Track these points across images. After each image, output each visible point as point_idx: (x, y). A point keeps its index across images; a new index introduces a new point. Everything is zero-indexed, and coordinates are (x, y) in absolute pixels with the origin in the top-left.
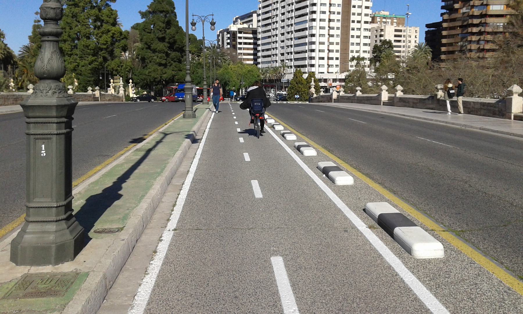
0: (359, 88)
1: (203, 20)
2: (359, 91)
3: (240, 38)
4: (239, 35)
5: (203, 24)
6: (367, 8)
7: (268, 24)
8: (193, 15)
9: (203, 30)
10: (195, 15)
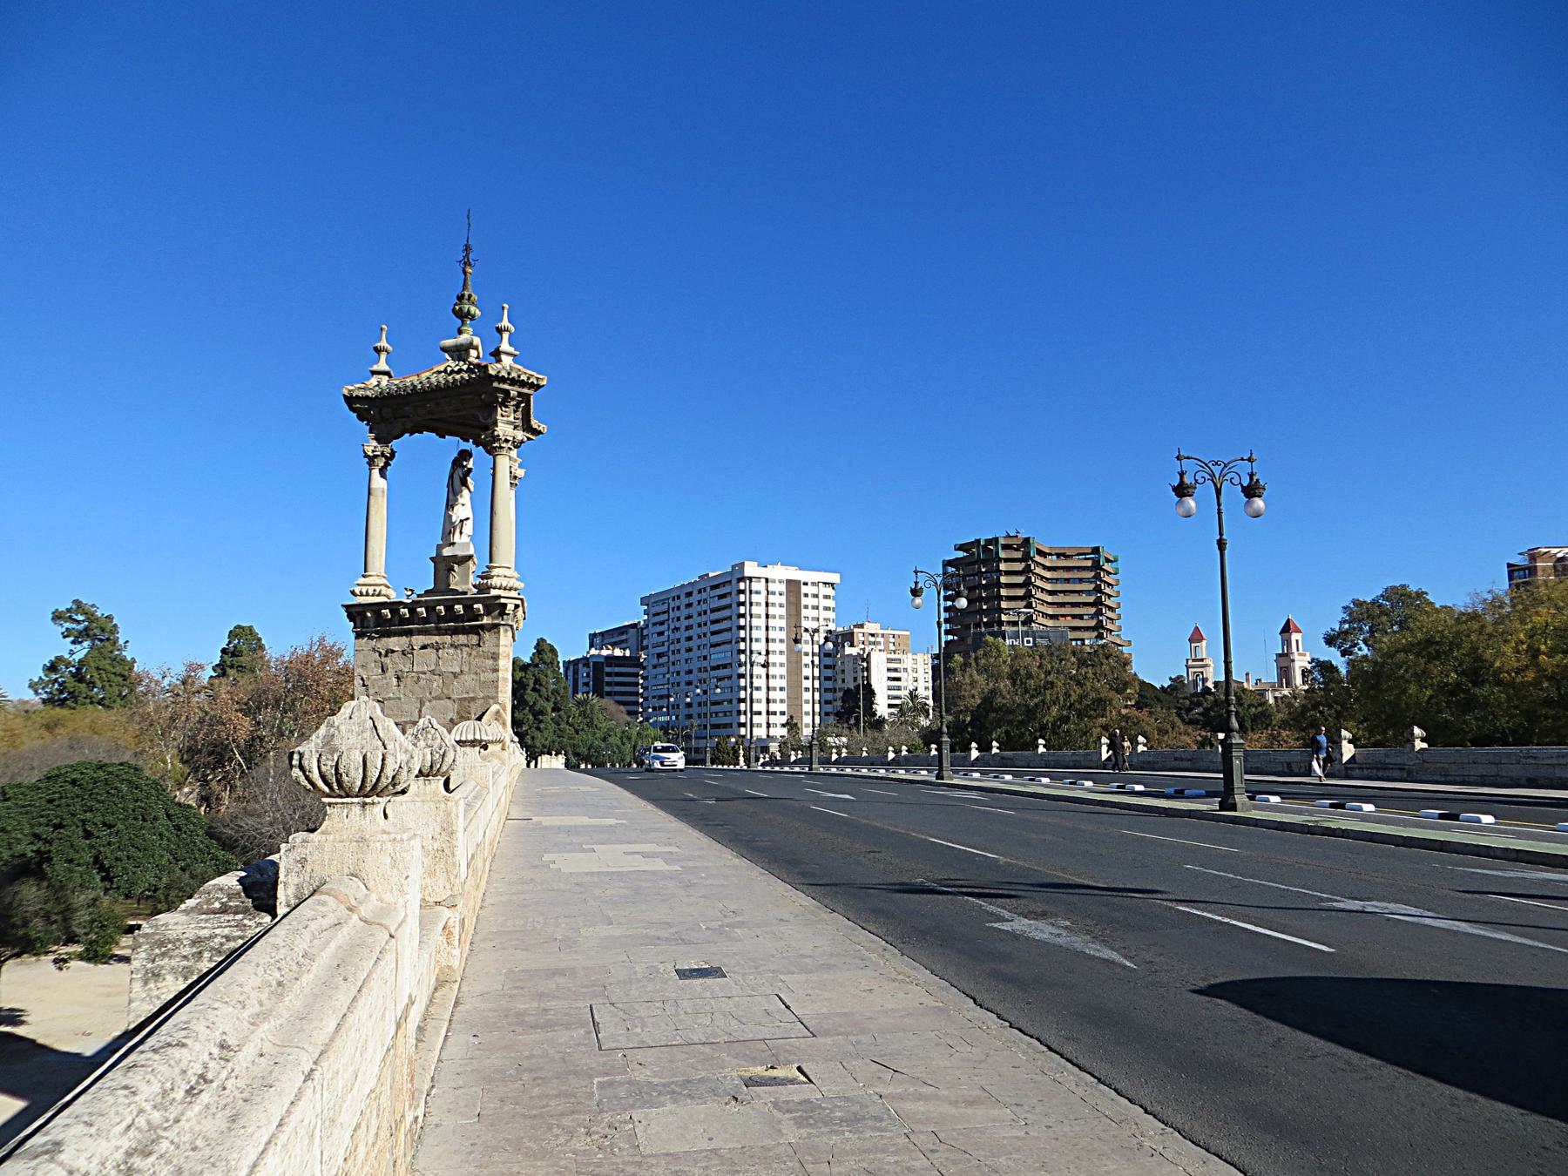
0: (1041, 741)
2: (1041, 747)
4: (607, 669)
5: (1218, 492)
6: (826, 609)
7: (1084, 567)
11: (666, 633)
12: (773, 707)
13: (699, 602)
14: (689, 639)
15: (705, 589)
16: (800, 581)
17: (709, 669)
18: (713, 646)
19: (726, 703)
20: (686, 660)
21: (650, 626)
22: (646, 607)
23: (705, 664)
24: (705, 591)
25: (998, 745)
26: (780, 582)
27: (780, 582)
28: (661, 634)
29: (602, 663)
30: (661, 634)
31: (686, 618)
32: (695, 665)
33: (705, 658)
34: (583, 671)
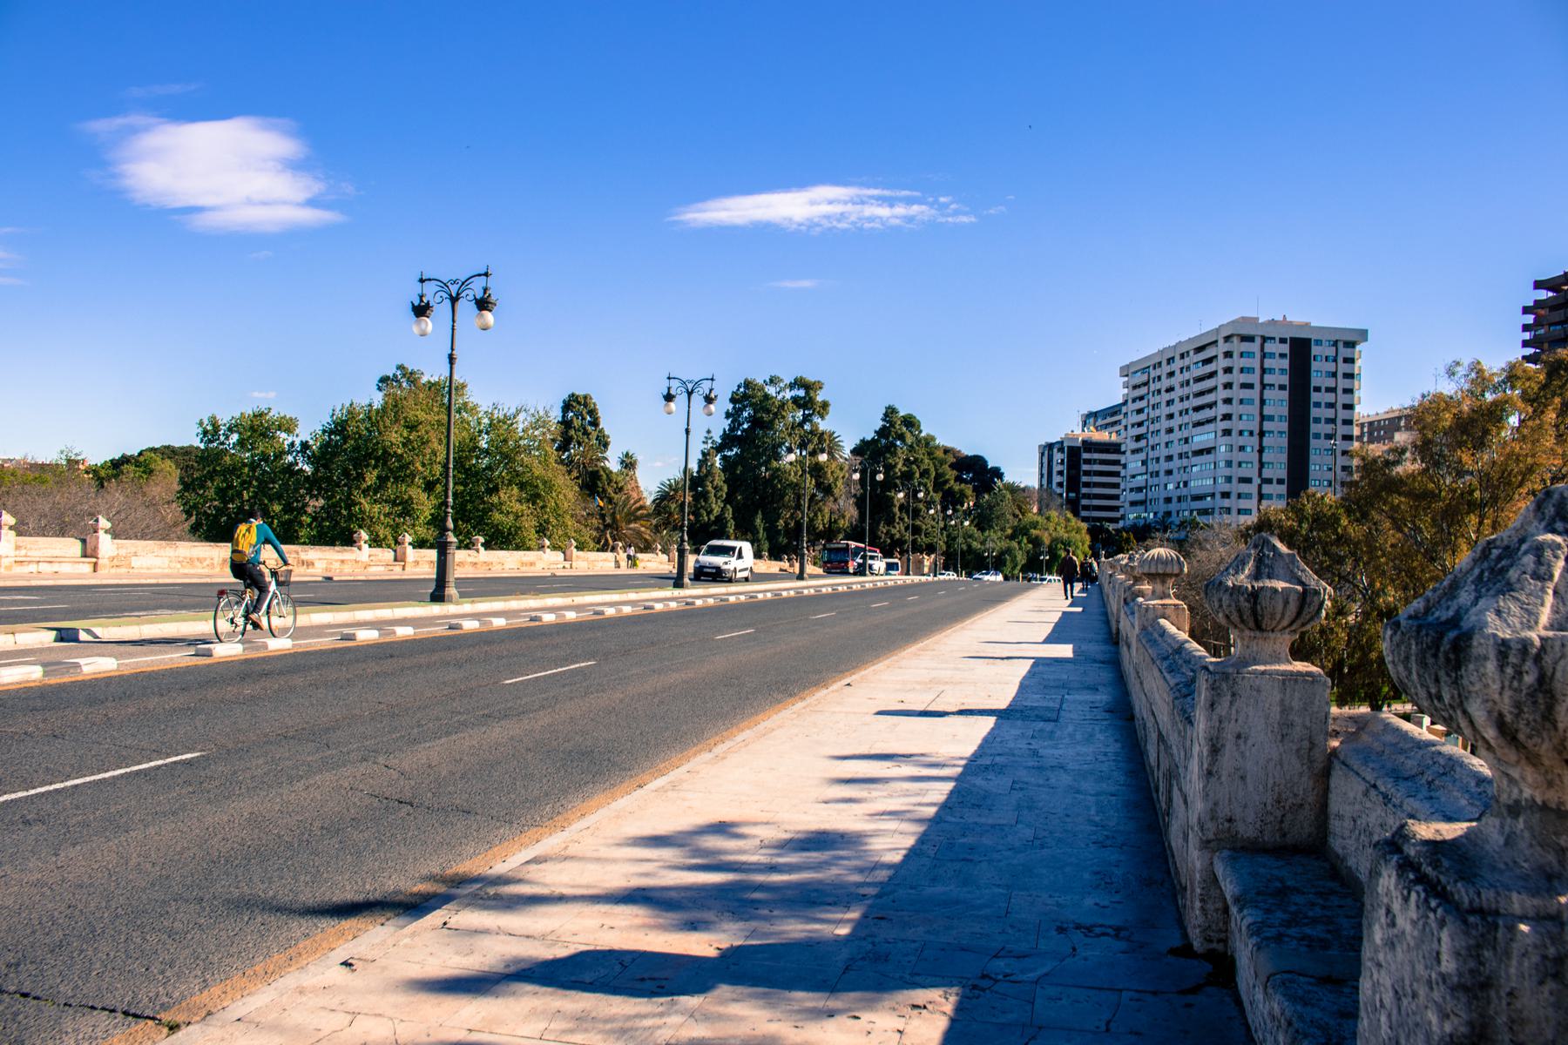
1: (454, 295)
3: (1088, 462)
4: (1085, 456)
8: (422, 281)
9: (453, 330)
10: (430, 280)
11: (1146, 411)
12: (1268, 379)
13: (1182, 369)
14: (1171, 416)
15: (1188, 352)
16: (1310, 340)
17: (1190, 454)
18: (1198, 424)
19: (1209, 499)
20: (1167, 444)
21: (1130, 401)
22: (1126, 379)
23: (1186, 448)
24: (1188, 355)
25: (109, 525)
26: (1283, 341)
27: (1283, 341)
28: (1140, 411)
29: (1079, 448)
30: (1140, 411)
31: (1173, 401)
32: (1175, 449)
33: (1187, 441)
34: (1058, 457)
